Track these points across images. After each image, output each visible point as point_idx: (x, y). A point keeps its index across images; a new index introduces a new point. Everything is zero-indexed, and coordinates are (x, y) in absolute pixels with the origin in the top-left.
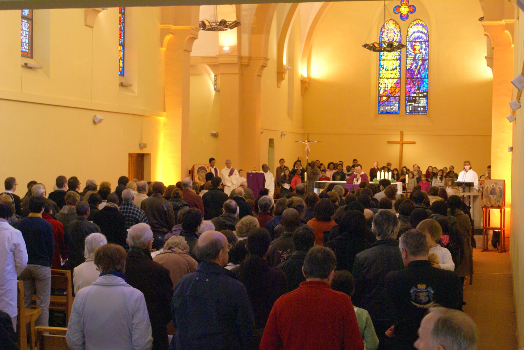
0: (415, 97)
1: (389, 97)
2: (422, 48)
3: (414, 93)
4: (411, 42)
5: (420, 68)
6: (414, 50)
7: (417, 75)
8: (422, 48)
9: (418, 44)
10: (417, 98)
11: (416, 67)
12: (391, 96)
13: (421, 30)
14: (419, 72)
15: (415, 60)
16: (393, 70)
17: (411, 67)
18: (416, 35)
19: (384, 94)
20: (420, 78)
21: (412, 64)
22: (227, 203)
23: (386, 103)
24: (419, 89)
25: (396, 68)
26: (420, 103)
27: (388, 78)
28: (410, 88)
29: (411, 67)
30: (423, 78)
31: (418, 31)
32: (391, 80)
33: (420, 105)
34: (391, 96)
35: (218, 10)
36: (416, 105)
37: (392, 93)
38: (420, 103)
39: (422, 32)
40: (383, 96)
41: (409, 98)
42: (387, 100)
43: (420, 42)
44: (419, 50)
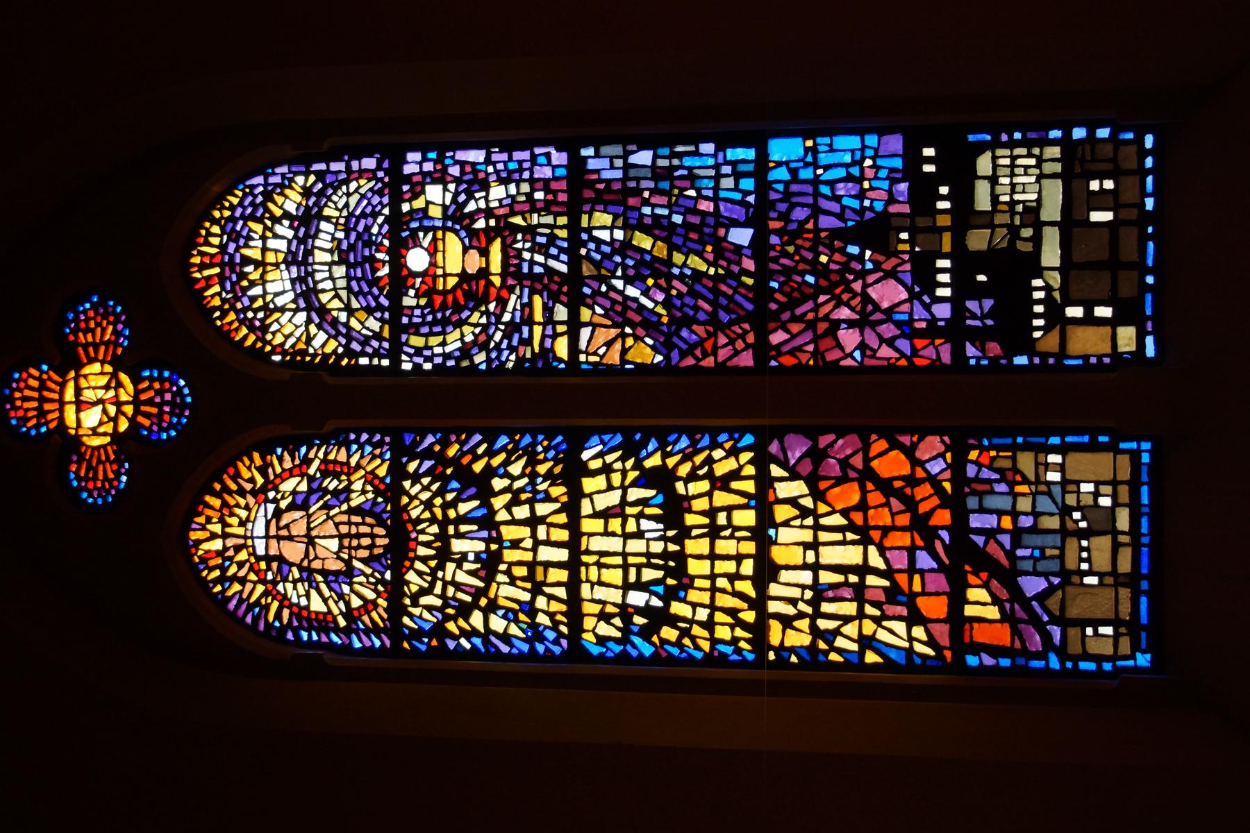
0: (965, 263)
1: (964, 560)
2: (456, 217)
3: (924, 280)
4: (398, 329)
5: (656, 227)
6: (473, 289)
7: (725, 252)
8: (456, 217)
9: (417, 260)
10: (978, 240)
11: (648, 269)
12: (960, 527)
13: (282, 238)
14: (704, 232)
15: (574, 278)
16: (674, 512)
17: (648, 323)
18: (330, 280)
19: (935, 607)
20: (756, 219)
21: (622, 314)
22: (1033, 635)
23: (1032, 585)
24: (875, 230)
25: (661, 479)
26: (1032, 213)
27: (767, 571)
28: (861, 323)
29: (648, 323)
30: (763, 186)
31: (299, 258)
32: (789, 543)
33: (1052, 210)
34: (960, 527)
35: (1109, 344)
36: (1051, 255)
37: (921, 525)
38: (1032, 213)
39: (307, 221)
40: (956, 619)
41: (980, 337)
42: (1004, 578)
43: (402, 233)
44: (477, 242)
